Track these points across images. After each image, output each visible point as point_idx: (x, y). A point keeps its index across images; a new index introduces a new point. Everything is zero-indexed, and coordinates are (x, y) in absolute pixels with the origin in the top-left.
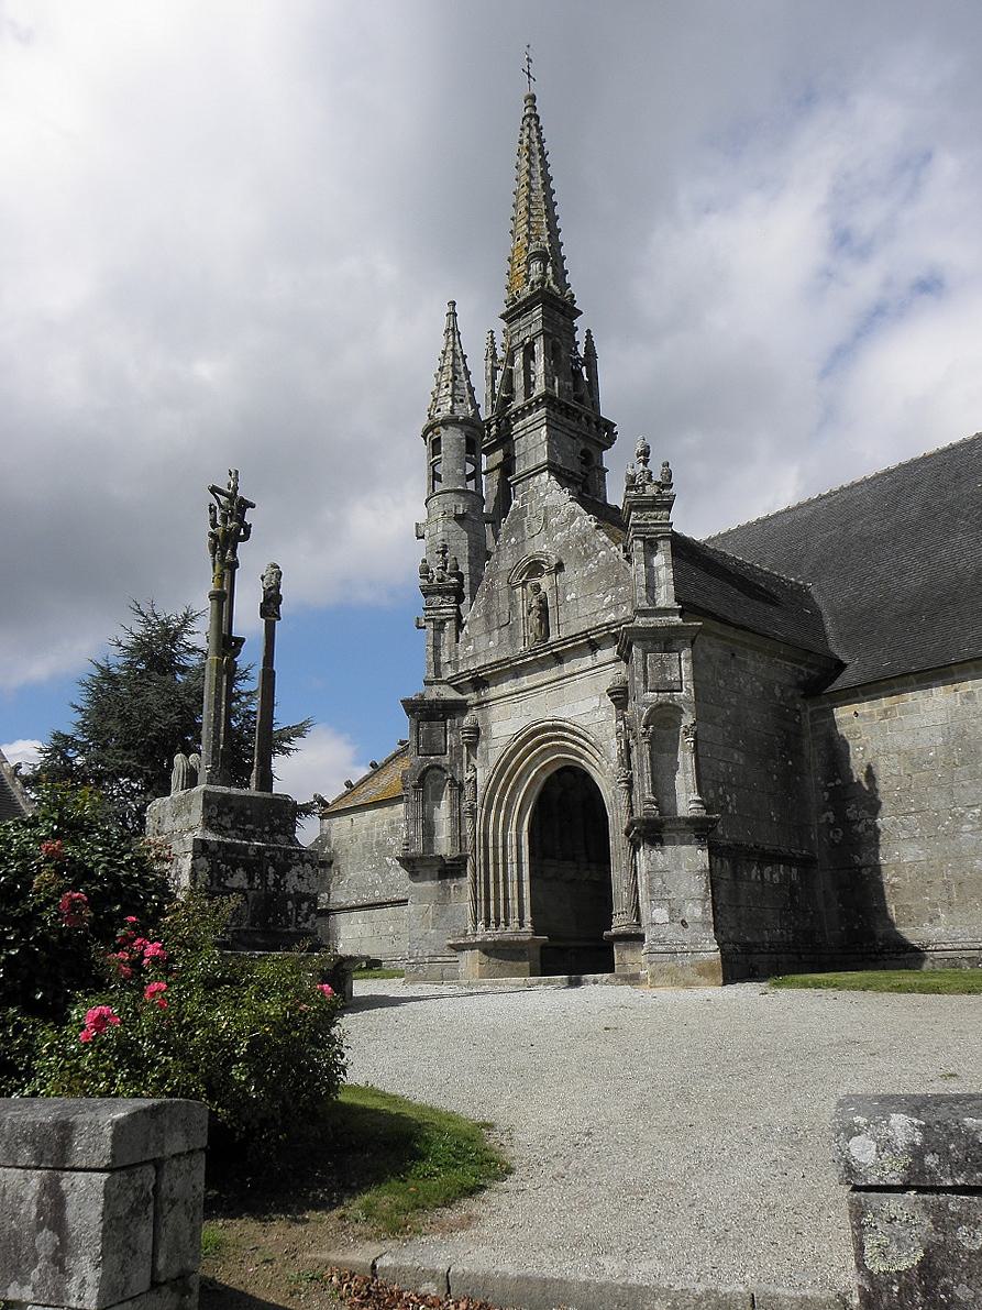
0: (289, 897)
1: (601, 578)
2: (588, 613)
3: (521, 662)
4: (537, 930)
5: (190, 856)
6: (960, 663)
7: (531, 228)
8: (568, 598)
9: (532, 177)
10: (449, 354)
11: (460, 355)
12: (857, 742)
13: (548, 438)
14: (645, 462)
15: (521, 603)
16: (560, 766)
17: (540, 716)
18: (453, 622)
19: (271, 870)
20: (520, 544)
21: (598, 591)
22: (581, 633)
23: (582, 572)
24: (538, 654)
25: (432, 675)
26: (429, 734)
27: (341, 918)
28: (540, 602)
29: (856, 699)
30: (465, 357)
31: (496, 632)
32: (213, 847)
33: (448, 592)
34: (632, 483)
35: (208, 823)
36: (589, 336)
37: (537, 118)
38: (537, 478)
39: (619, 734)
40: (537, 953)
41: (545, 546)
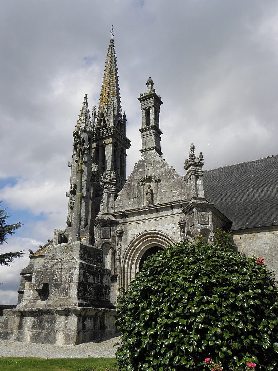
1: (175, 186)
3: (143, 210)
5: (78, 269)
6: (261, 227)
7: (110, 78)
9: (111, 63)
10: (85, 110)
11: (88, 111)
12: (241, 246)
13: (155, 139)
14: (193, 152)
16: (153, 246)
17: (149, 229)
18: (114, 194)
19: (99, 276)
20: (143, 172)
21: (174, 190)
22: (169, 203)
24: (150, 208)
25: (106, 211)
26: (105, 231)
29: (240, 233)
30: (89, 112)
33: (113, 184)
35: (81, 257)
36: (124, 114)
37: (114, 46)
38: (150, 151)
39: (182, 237)
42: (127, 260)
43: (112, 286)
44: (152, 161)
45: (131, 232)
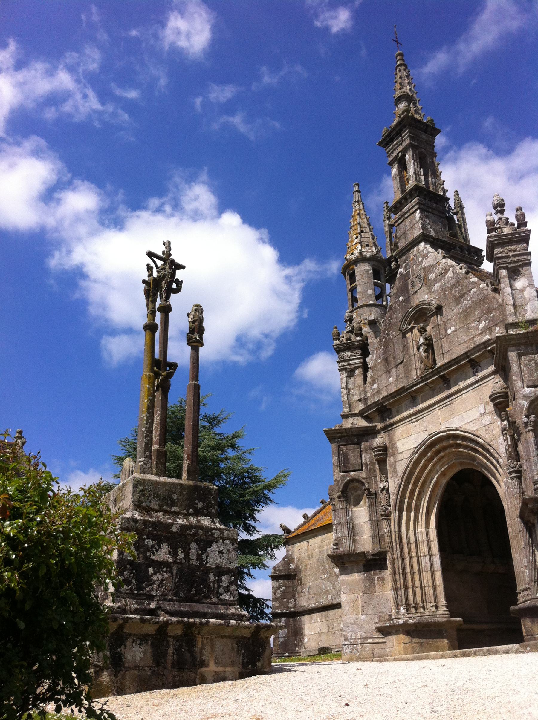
0: (208, 570)
2: (466, 339)
4: (452, 614)
8: (449, 331)
13: (421, 219)
15: (411, 344)
19: (193, 545)
20: (407, 300)
21: (474, 321)
23: (457, 310)
25: (346, 410)
27: (306, 618)
28: (426, 339)
31: (394, 370)
32: (140, 526)
33: (356, 348)
34: (491, 227)
35: (138, 506)
39: (505, 432)
40: (454, 633)
41: (426, 296)
42: (405, 513)
43: (378, 578)
44: (420, 270)
45: (403, 444)
